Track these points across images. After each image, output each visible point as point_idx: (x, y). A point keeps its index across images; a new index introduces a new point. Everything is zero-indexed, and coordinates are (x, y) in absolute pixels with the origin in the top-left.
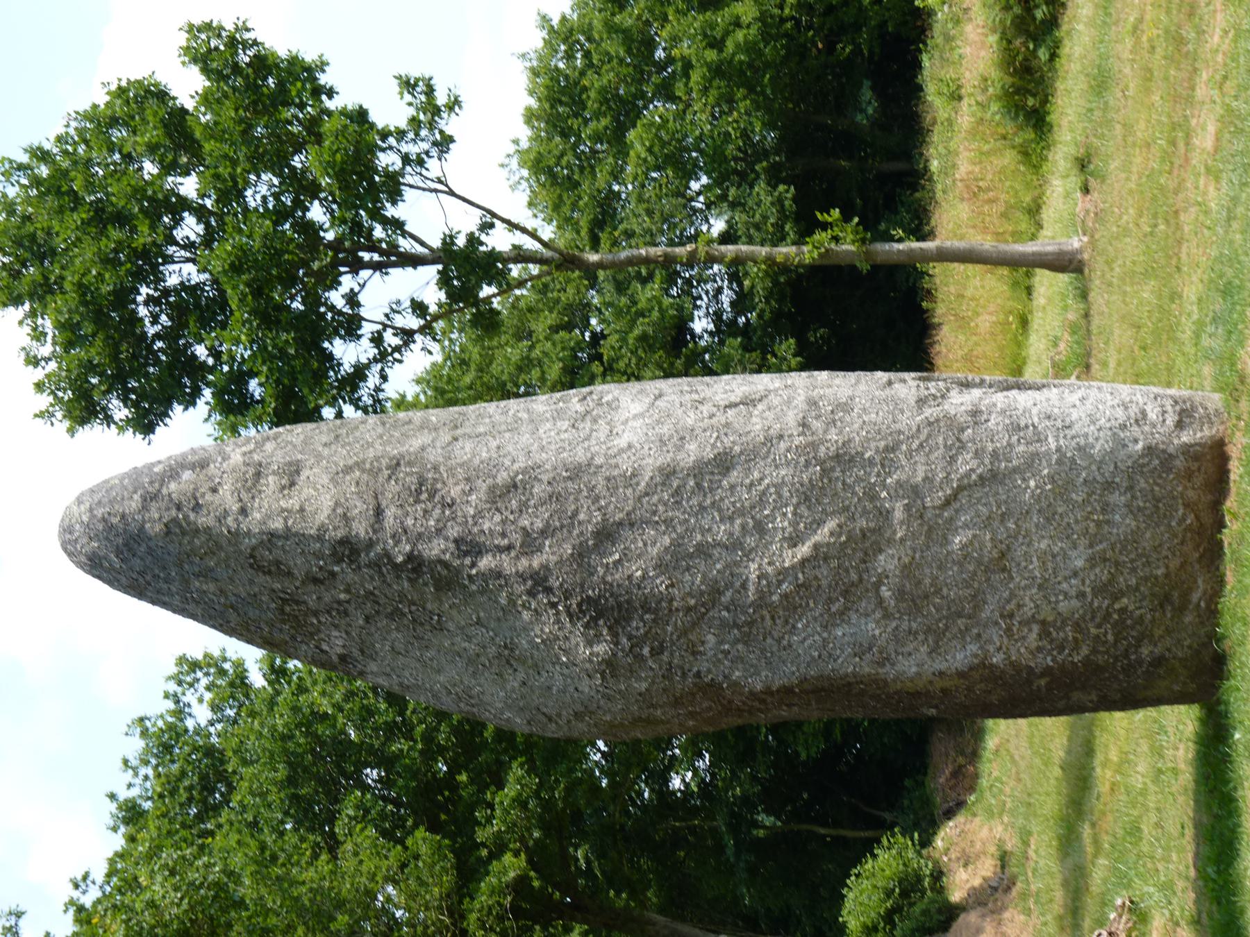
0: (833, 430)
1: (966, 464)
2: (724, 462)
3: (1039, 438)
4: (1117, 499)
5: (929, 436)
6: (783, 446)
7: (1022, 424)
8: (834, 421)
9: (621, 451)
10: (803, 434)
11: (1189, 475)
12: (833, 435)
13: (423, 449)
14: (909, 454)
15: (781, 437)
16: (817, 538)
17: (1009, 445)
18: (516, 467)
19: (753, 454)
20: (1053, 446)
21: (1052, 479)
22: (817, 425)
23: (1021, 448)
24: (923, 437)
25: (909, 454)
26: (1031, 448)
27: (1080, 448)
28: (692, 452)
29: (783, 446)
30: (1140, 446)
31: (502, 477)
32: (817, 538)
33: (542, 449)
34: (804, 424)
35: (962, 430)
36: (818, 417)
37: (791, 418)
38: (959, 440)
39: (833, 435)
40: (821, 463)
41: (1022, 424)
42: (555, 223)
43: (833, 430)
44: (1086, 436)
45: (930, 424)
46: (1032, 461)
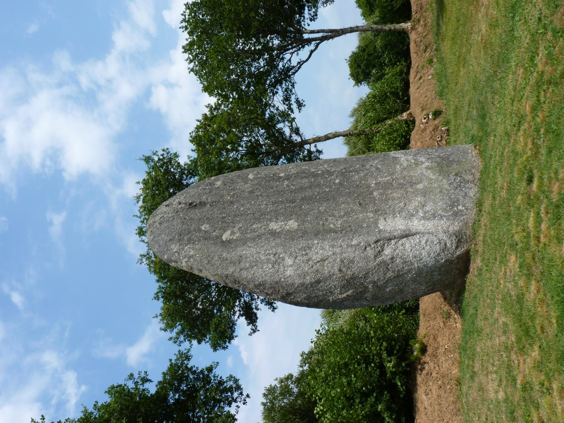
0: (349, 270)
1: (390, 274)
2: (318, 282)
3: (412, 264)
4: (436, 273)
5: (378, 269)
6: (334, 277)
7: (407, 261)
8: (349, 268)
9: (288, 277)
10: (340, 273)
11: (458, 263)
12: (349, 273)
13: (233, 273)
14: (372, 274)
15: (334, 275)
16: (347, 293)
17: (403, 267)
18: (260, 280)
19: (326, 280)
20: (416, 266)
21: (416, 274)
22: (344, 269)
23: (407, 268)
24: (376, 269)
25: (372, 274)
26: (410, 267)
27: (424, 265)
28: (308, 280)
29: (334, 277)
30: (443, 261)
31: (257, 283)
32: (347, 293)
33: (266, 275)
34: (340, 270)
35: (388, 265)
36: (344, 267)
37: (336, 269)
38: (387, 268)
39: (349, 273)
40: (347, 280)
41: (407, 261)
42: (377, 13)
43: (349, 270)
44: (427, 261)
45: (378, 265)
46: (409, 271)
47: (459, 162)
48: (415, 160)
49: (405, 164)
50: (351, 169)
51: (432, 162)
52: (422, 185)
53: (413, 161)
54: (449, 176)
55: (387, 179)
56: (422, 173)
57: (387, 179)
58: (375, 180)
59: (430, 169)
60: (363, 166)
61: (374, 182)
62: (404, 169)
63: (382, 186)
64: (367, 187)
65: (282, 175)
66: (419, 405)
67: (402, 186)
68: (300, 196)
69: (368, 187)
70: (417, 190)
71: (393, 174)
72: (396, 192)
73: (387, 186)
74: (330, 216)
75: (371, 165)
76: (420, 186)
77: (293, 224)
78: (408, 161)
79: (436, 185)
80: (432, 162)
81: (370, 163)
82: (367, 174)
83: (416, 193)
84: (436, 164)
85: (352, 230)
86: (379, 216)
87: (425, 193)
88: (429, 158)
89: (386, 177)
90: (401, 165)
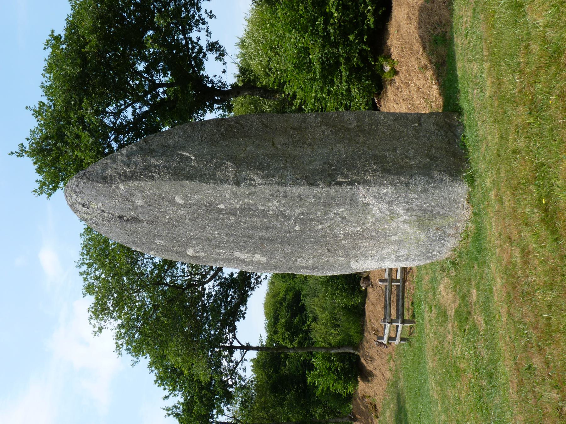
47: (444, 217)
48: (390, 211)
49: (378, 215)
50: (311, 216)
51: (411, 216)
52: (397, 236)
53: (388, 213)
54: (428, 230)
55: (356, 229)
56: (398, 227)
57: (356, 229)
58: (343, 230)
59: (408, 223)
60: (325, 214)
61: (342, 232)
62: (377, 221)
63: (351, 236)
64: (334, 237)
65: (221, 206)
66: (393, 17)
67: (374, 238)
68: (257, 234)
69: (336, 237)
70: (391, 241)
71: (363, 224)
72: (367, 242)
73: (356, 237)
74: (299, 258)
75: (336, 214)
76: (393, 238)
77: (263, 259)
78: (381, 212)
79: (412, 237)
80: (411, 216)
81: (334, 211)
82: (332, 224)
83: (390, 243)
84: (416, 218)
85: (324, 268)
86: (350, 259)
87: (399, 243)
88: (408, 210)
89: (355, 227)
90: (373, 215)
